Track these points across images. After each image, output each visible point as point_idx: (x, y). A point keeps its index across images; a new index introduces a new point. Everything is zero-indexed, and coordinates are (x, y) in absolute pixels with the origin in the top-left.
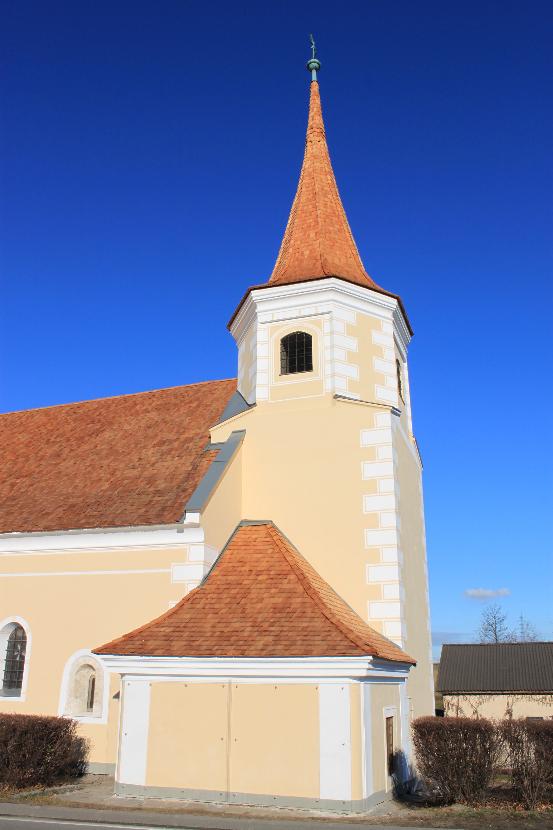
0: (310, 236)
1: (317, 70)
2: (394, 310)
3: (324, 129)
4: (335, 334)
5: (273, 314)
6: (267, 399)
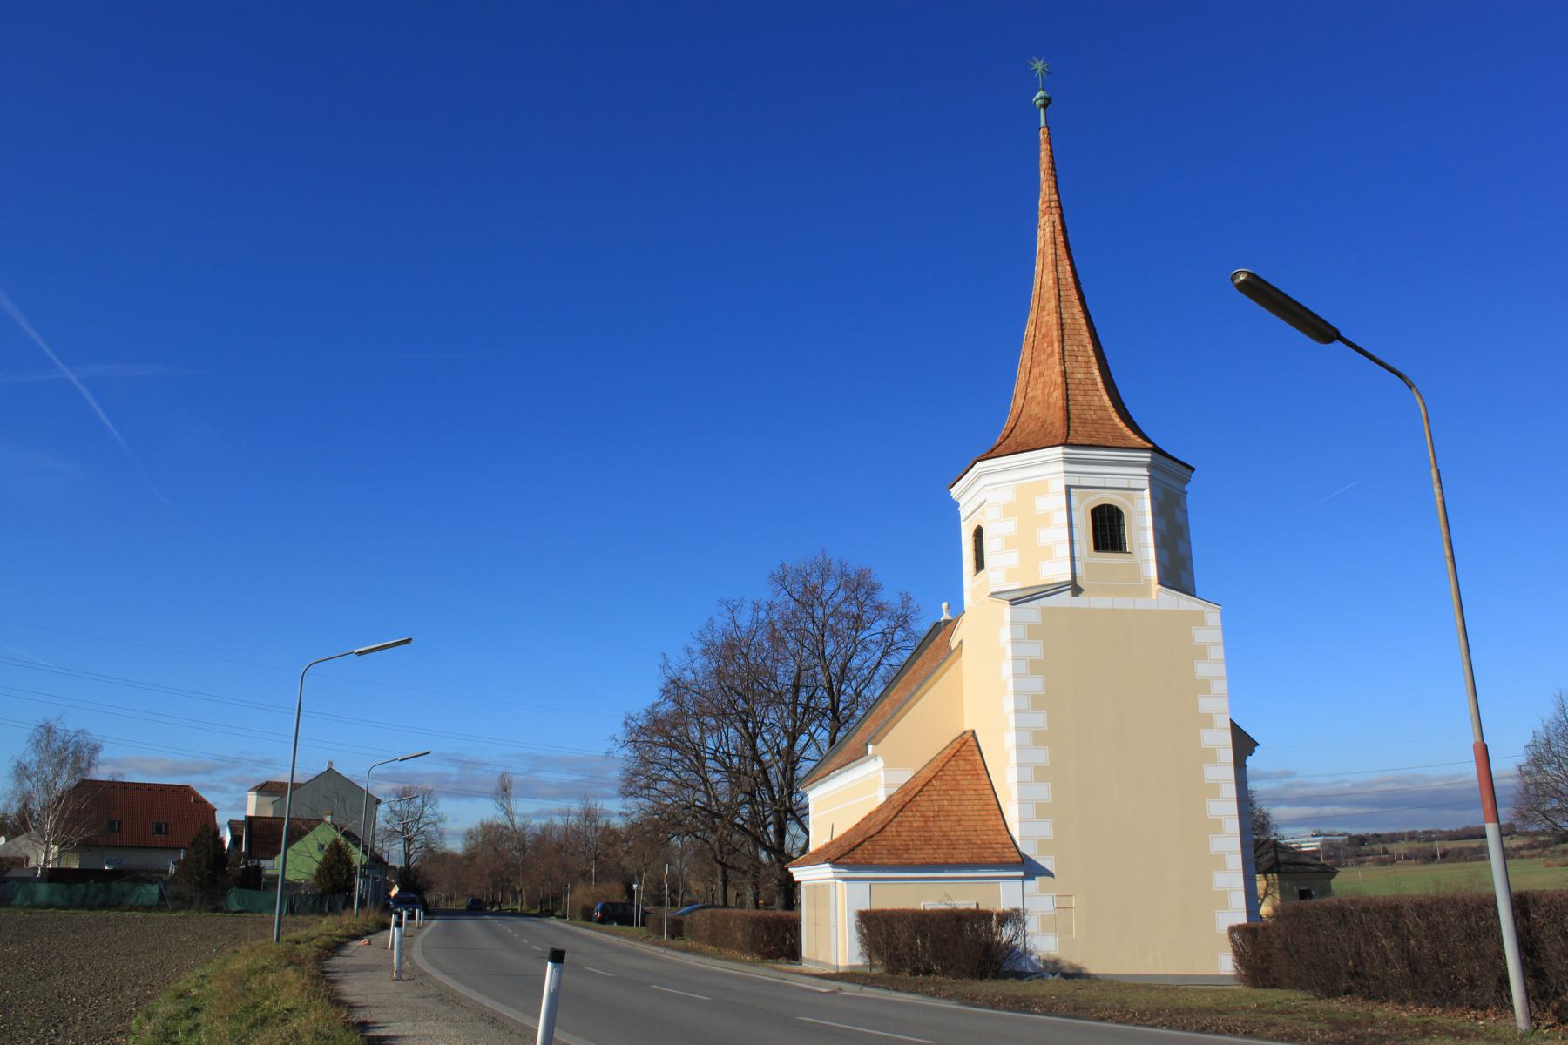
1: (1045, 106)
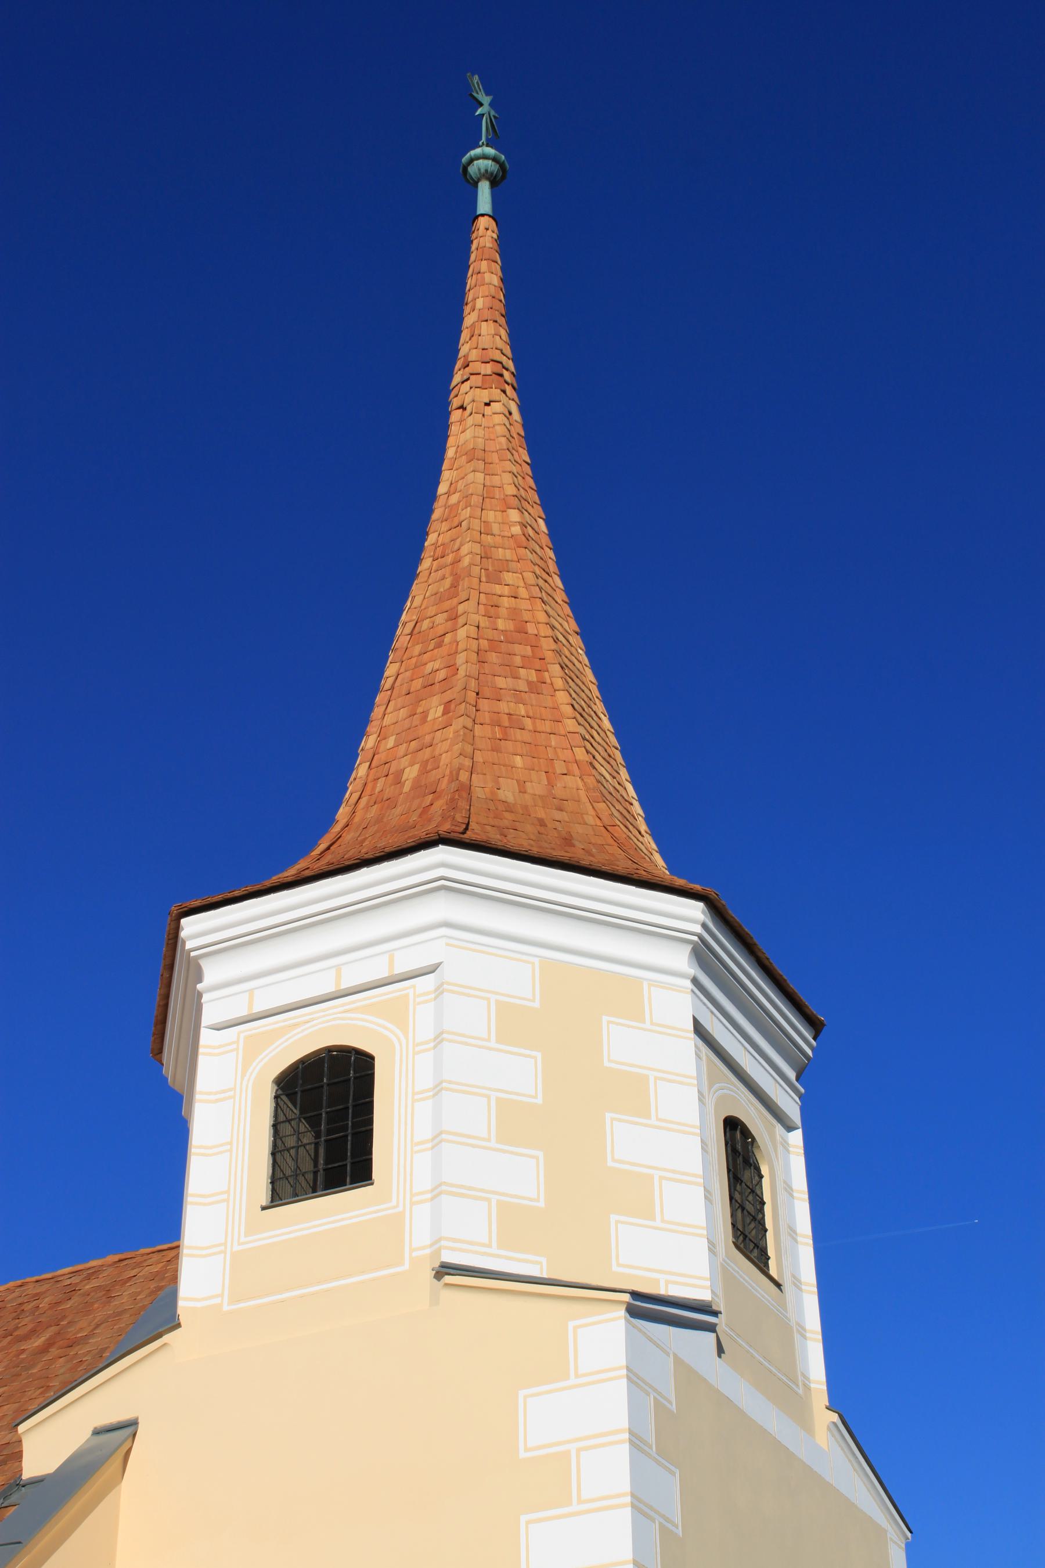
0: (427, 716)
1: (495, 182)
2: (696, 938)
3: (510, 365)
4: (450, 1041)
5: (251, 991)
6: (218, 1301)
